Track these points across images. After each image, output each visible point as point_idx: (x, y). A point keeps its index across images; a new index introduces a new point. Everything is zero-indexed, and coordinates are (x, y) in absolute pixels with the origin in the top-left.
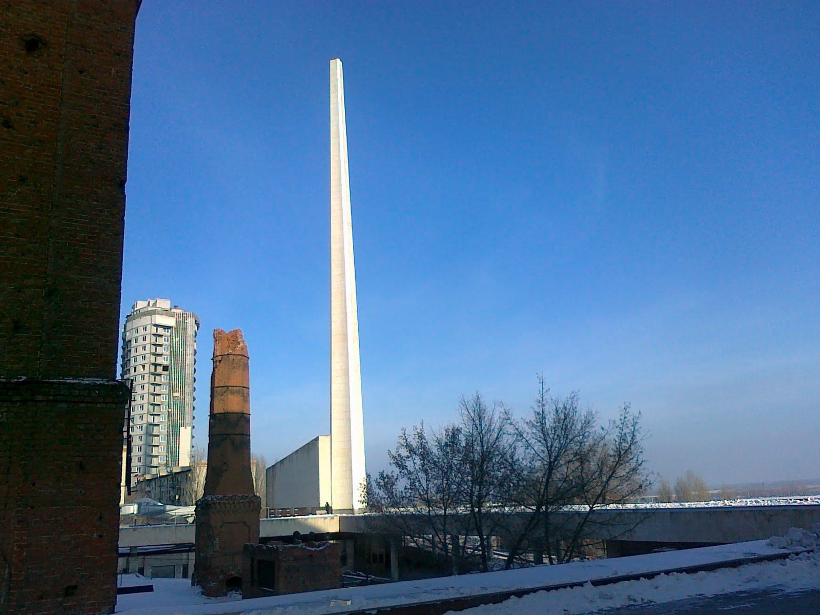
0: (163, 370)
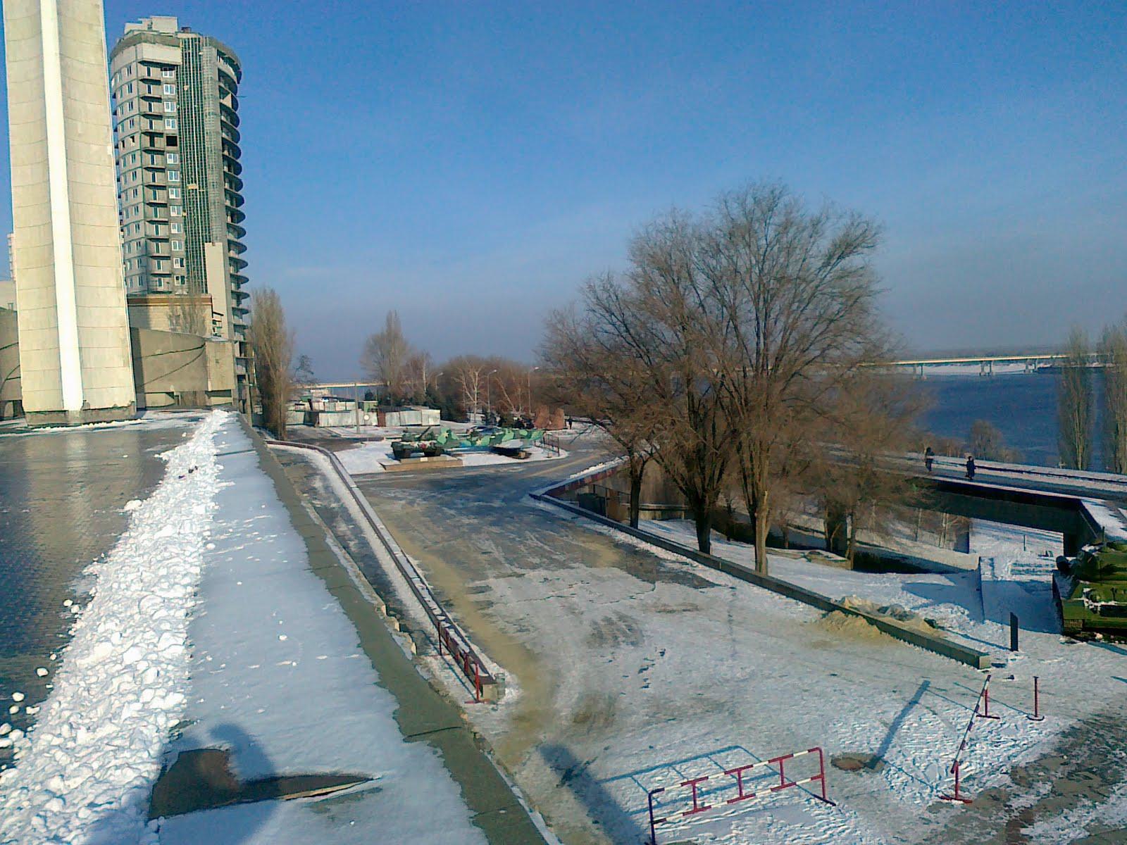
0: (168, 145)
